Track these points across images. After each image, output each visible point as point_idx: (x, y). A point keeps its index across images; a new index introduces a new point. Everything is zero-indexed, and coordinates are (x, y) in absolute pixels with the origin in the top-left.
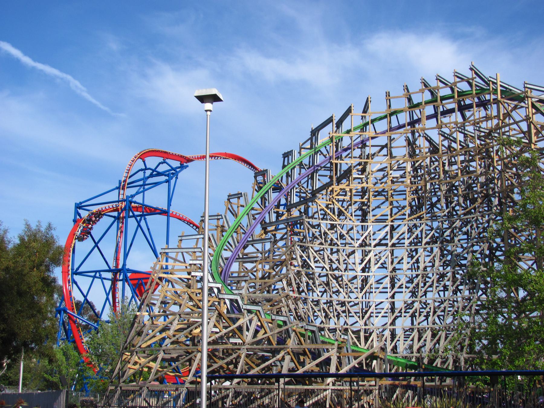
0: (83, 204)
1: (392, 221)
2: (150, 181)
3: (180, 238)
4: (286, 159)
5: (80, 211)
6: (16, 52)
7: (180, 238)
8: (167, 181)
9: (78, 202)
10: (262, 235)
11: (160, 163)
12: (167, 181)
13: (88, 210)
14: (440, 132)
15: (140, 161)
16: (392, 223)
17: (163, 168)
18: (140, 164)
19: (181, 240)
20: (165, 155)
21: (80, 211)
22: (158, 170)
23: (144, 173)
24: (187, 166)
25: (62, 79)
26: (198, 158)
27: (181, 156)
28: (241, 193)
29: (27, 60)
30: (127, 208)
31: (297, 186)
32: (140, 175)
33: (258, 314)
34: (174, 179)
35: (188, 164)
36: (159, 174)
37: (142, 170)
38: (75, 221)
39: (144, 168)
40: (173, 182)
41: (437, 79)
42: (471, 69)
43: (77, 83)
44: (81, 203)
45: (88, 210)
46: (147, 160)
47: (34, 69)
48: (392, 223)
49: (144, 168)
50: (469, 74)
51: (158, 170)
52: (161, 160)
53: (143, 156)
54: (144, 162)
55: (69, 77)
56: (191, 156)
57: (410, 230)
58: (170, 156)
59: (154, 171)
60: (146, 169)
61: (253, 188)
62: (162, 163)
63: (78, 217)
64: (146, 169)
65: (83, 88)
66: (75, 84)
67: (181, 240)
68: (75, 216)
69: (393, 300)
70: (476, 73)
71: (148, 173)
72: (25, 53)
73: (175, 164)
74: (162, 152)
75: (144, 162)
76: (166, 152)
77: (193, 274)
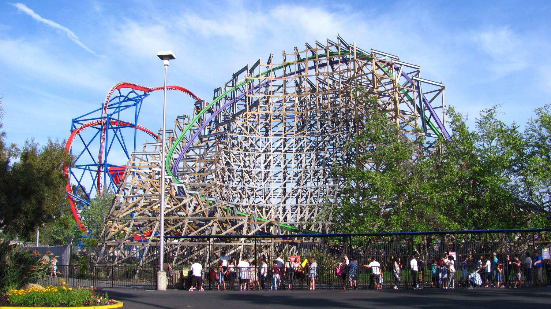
0: (77, 120)
1: (285, 136)
2: (123, 104)
3: (145, 145)
4: (216, 93)
5: (75, 124)
6: (29, 11)
7: (145, 145)
8: (135, 105)
9: (74, 118)
10: (199, 143)
11: (130, 93)
12: (135, 105)
13: (82, 124)
15: (117, 90)
16: (285, 137)
17: (132, 96)
18: (116, 93)
19: (145, 147)
20: (134, 87)
21: (75, 124)
22: (129, 97)
23: (120, 99)
24: (149, 95)
25: (62, 30)
26: (156, 89)
27: (145, 88)
28: (186, 116)
29: (37, 17)
30: (108, 123)
31: (223, 111)
32: (117, 100)
33: (197, 196)
34: (140, 103)
35: (150, 93)
36: (129, 100)
37: (118, 97)
38: (72, 131)
39: (119, 95)
40: (139, 105)
41: (316, 44)
42: (338, 38)
43: (72, 34)
44: (76, 119)
45: (82, 124)
46: (122, 90)
47: (42, 23)
48: (285, 137)
49: (119, 95)
50: (337, 42)
51: (129, 97)
52: (131, 90)
53: (119, 87)
54: (119, 91)
55: (66, 29)
56: (151, 87)
57: (297, 142)
58: (138, 88)
59: (126, 97)
60: (121, 96)
61: (194, 112)
62: (132, 92)
63: (74, 128)
64: (121, 96)
65: (77, 38)
66: (71, 34)
67: (145, 147)
68: (72, 128)
69: (285, 187)
70: (341, 41)
71: (122, 99)
72: (36, 12)
73: (141, 93)
74: (132, 84)
75: (119, 91)
76: (134, 85)
77: (153, 169)
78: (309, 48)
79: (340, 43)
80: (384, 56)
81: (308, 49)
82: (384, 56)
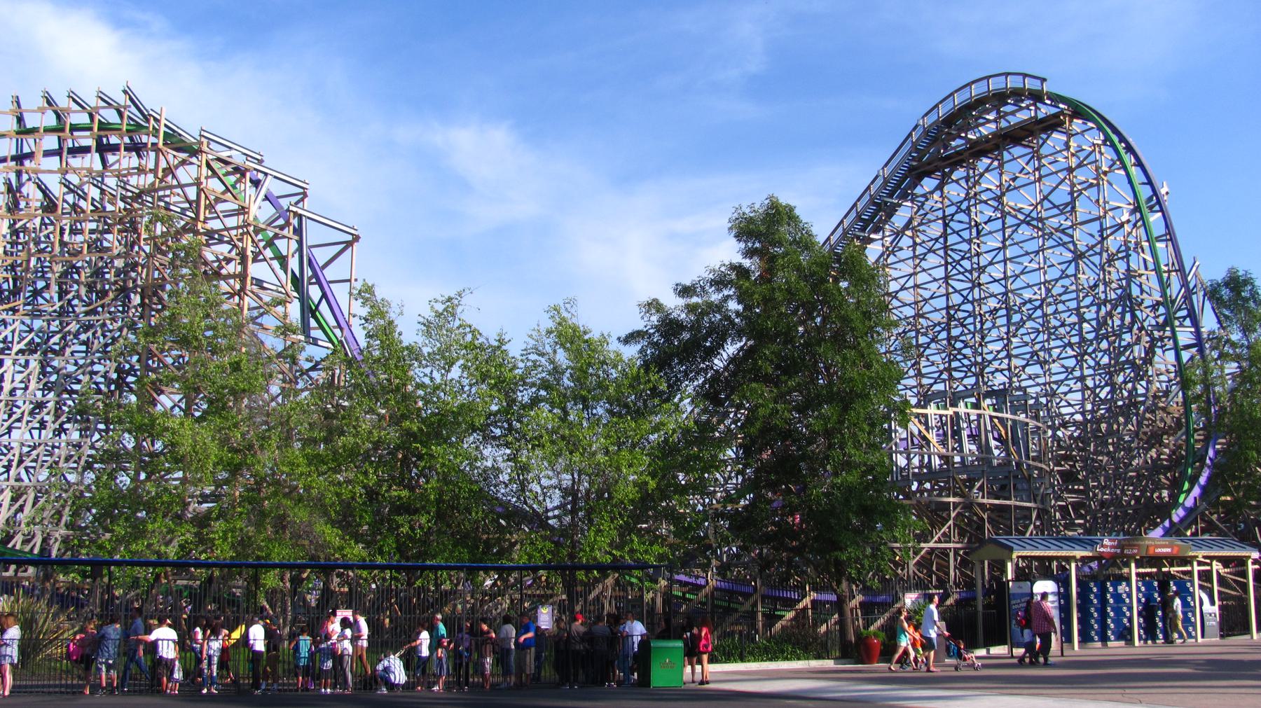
14: (63, 181)
41: (69, 97)
42: (125, 92)
50: (122, 99)
78: (48, 102)
79: (129, 103)
80: (230, 148)
81: (46, 105)
82: (230, 148)
